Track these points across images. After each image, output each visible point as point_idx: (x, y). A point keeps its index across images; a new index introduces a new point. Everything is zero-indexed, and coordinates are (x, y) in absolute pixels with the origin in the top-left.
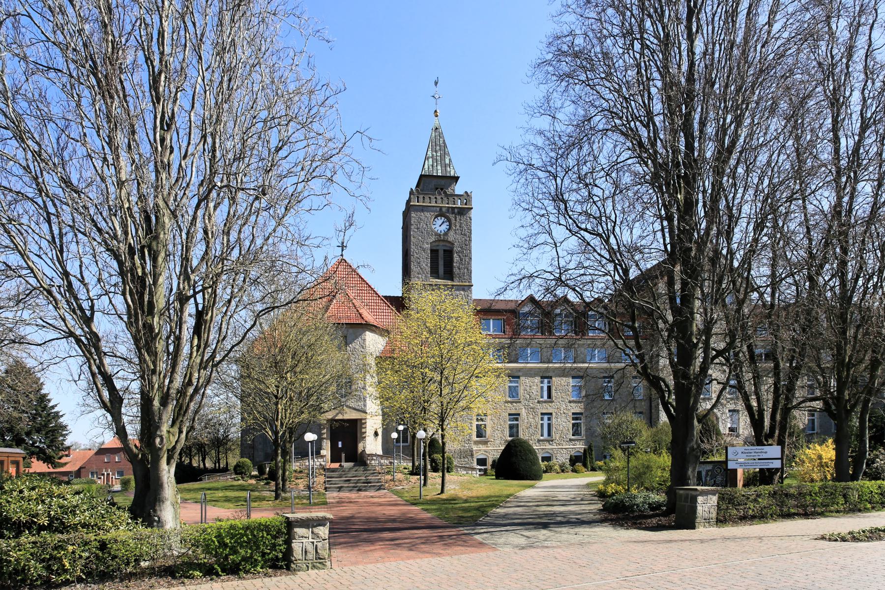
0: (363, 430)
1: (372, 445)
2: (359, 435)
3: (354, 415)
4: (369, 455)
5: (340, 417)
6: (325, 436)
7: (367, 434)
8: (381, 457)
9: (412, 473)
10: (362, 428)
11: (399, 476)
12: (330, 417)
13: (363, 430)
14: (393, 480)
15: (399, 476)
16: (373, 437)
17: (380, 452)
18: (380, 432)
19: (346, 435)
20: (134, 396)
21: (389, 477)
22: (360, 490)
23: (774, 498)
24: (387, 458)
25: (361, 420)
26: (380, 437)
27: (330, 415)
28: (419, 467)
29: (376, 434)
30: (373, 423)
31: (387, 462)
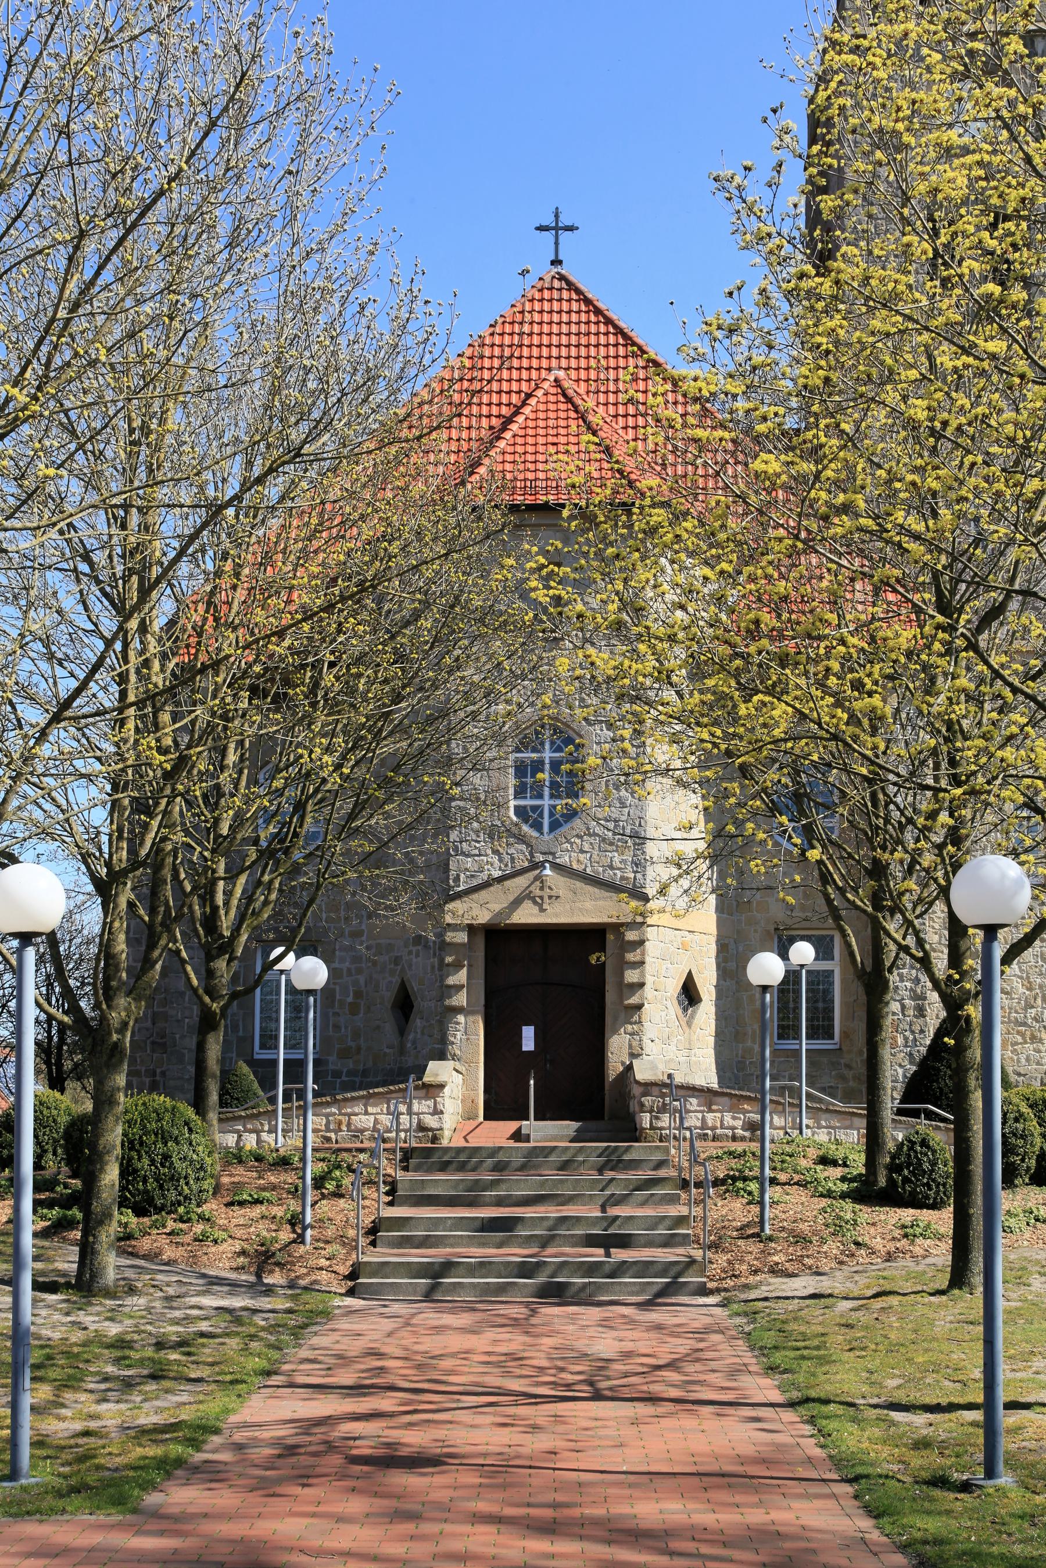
0: (631, 976)
1: (668, 1042)
2: (610, 997)
3: (575, 907)
4: (648, 1086)
5: (526, 915)
6: (461, 999)
7: (648, 991)
8: (706, 1095)
9: (866, 1192)
10: (623, 965)
11: (791, 1206)
12: (483, 917)
13: (631, 976)
14: (754, 1232)
15: (791, 1206)
16: (674, 1009)
17: (707, 1075)
18: (707, 985)
19: (556, 994)
20: (304, 427)
21: (734, 1210)
22: (555, 1293)
23: (643, 954)
24: (735, 1103)
25: (617, 928)
26: (707, 1011)
27: (479, 910)
28: (911, 1158)
29: (689, 994)
30: (678, 942)
31: (734, 1122)
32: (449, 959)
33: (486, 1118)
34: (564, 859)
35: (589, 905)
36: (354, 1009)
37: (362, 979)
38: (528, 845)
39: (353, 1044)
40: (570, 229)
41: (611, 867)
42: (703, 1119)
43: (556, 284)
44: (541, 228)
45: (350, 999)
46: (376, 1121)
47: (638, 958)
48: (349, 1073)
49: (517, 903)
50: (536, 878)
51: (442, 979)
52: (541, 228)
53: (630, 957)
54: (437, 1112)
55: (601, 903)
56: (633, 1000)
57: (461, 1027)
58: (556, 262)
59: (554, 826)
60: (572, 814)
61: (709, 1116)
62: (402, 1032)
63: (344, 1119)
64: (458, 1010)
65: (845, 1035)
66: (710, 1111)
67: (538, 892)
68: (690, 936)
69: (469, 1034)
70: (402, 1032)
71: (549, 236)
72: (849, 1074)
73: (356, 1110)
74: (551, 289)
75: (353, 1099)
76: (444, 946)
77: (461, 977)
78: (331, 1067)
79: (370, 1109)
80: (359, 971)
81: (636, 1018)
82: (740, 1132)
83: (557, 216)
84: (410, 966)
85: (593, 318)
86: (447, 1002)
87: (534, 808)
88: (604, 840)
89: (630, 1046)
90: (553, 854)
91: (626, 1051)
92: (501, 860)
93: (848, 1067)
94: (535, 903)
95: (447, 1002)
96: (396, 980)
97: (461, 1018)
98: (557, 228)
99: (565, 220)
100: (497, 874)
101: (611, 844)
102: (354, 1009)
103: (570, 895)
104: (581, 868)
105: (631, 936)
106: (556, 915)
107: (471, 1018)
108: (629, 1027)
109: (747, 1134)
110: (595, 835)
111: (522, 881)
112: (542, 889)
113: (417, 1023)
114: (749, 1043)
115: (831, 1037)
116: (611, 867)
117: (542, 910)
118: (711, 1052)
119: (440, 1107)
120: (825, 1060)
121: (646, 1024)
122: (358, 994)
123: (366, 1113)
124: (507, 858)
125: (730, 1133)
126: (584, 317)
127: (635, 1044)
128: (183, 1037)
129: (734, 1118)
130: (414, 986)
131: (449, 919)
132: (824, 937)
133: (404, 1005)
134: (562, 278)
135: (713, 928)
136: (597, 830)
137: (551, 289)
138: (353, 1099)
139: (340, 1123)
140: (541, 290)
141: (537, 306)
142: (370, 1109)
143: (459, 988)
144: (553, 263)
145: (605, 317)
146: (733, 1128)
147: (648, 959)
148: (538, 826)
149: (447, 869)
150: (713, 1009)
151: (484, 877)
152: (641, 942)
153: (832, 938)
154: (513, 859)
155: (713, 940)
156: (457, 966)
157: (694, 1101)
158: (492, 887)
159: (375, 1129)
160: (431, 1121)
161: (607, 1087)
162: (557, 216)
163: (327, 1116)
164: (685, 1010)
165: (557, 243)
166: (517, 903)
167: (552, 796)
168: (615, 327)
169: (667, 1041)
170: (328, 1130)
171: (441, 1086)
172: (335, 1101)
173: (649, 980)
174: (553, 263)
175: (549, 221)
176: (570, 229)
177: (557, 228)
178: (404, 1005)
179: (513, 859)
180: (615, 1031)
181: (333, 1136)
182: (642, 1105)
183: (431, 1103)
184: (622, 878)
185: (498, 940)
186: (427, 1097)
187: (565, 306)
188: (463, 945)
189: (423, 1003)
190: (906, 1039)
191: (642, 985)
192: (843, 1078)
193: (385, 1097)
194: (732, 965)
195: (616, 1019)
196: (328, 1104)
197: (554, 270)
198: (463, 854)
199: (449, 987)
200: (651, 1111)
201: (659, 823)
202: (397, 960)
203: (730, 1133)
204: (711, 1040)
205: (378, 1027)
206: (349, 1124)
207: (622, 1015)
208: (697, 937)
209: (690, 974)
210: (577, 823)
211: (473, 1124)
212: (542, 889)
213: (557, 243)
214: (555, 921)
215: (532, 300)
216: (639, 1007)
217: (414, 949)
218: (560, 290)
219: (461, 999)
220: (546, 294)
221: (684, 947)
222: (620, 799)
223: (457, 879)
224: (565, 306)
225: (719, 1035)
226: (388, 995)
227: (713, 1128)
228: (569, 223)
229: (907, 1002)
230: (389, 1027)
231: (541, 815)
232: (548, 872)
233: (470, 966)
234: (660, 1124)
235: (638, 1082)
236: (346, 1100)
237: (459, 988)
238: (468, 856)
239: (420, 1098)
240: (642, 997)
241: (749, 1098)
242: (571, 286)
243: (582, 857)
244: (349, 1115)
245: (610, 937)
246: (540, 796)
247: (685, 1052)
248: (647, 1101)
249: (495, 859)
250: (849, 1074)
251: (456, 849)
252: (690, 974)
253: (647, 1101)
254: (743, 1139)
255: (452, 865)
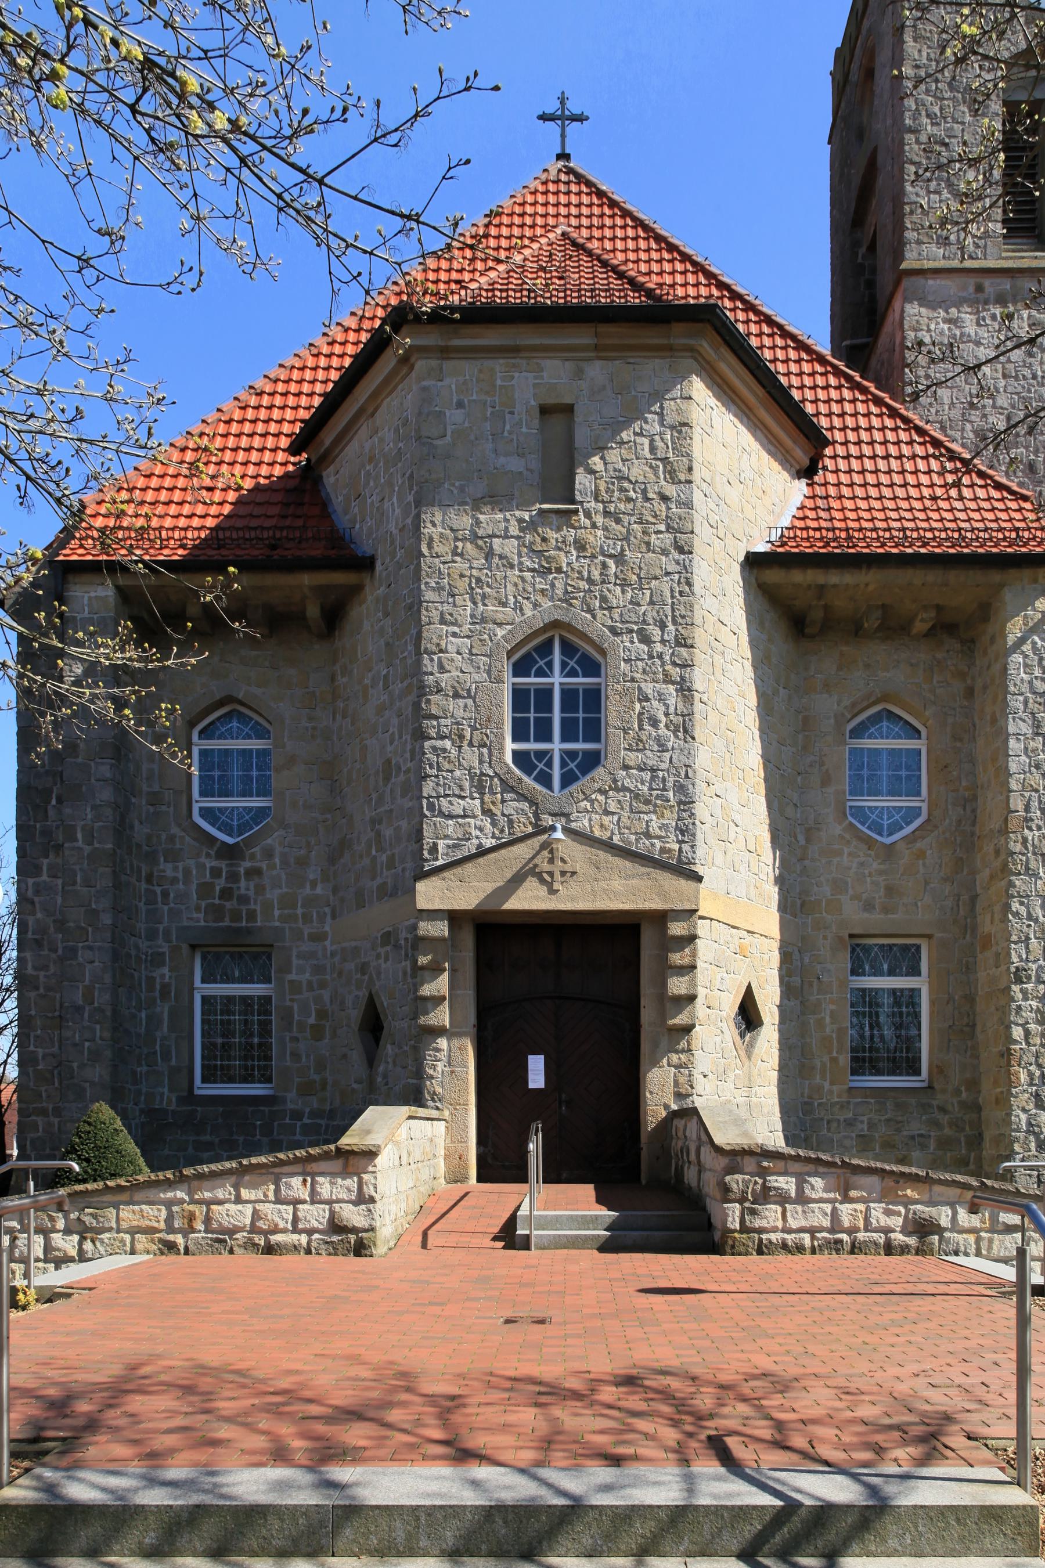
0: (677, 986)
1: (727, 1081)
2: (647, 1015)
5: (530, 899)
6: (442, 1016)
10: (666, 970)
13: (677, 986)
16: (730, 1031)
23: (694, 955)
25: (661, 918)
29: (748, 1016)
32: (423, 960)
33: (480, 1179)
34: (582, 823)
35: (617, 884)
36: (317, 1032)
37: (326, 995)
38: (532, 803)
39: (317, 1077)
40: (580, 118)
41: (648, 835)
42: (835, 1214)
43: (563, 177)
44: (544, 117)
45: (312, 1020)
46: (256, 1214)
47: (686, 961)
48: (313, 1114)
49: (517, 881)
50: (544, 846)
51: (416, 987)
52: (544, 117)
53: (677, 958)
54: (363, 1199)
55: (635, 882)
56: (680, 1020)
57: (443, 1055)
58: (563, 156)
59: (568, 780)
60: (592, 761)
61: (846, 1210)
62: (371, 1060)
63: (199, 1211)
64: (439, 1031)
65: (938, 1069)
66: (847, 1199)
67: (546, 866)
68: (749, 938)
69: (454, 1065)
70: (371, 1060)
71: (553, 127)
72: (944, 1119)
73: (220, 1194)
74: (557, 182)
75: (213, 1175)
76: (419, 943)
77: (441, 985)
78: (290, 1106)
79: (245, 1194)
80: (323, 985)
81: (683, 1044)
82: (898, 1237)
83: (563, 103)
84: (379, 973)
85: (607, 211)
86: (422, 1020)
87: (541, 755)
88: (637, 796)
89: (676, 1083)
90: (567, 816)
91: (670, 1089)
92: (494, 824)
93: (942, 1109)
94: (542, 881)
95: (422, 1020)
96: (363, 994)
97: (443, 1043)
98: (562, 117)
99: (574, 107)
100: (489, 842)
101: (647, 802)
102: (317, 1032)
103: (592, 871)
104: (605, 835)
105: (676, 929)
106: (573, 900)
107: (456, 1042)
108: (675, 1058)
109: (912, 1241)
110: (625, 789)
111: (523, 851)
112: (551, 861)
113: (389, 1049)
114: (818, 1080)
115: (918, 1073)
116: (648, 835)
117: (552, 892)
118: (774, 1090)
119: (369, 1190)
120: (913, 1101)
121: (698, 1053)
122: (322, 1014)
123: (238, 1200)
124: (503, 821)
125: (881, 1238)
126: (596, 211)
127: (682, 1080)
128: (82, 1066)
129: (888, 1213)
130: (384, 1001)
131: (422, 903)
132: (905, 948)
133: (373, 1025)
134: (570, 171)
135: (776, 932)
136: (627, 783)
137: (557, 182)
138: (213, 1175)
139: (191, 1217)
140: (545, 183)
141: (541, 199)
142: (245, 1194)
143: (439, 1000)
144: (559, 157)
145: (621, 209)
146: (887, 1231)
147: (700, 964)
148: (545, 779)
149: (418, 836)
150: (776, 1036)
151: (471, 847)
152: (692, 938)
153: (918, 948)
154: (511, 823)
155: (775, 945)
156: (436, 970)
157: (818, 1182)
158: (480, 852)
159: (254, 1229)
160: (353, 1215)
161: (644, 1139)
162: (563, 103)
163: (169, 1204)
164: (742, 1035)
165: (563, 136)
166: (517, 881)
167: (564, 739)
168: (634, 219)
169: (722, 1076)
170: (170, 1229)
171: (371, 1154)
172: (182, 1179)
173: (701, 992)
174: (559, 157)
175: (552, 107)
176: (580, 118)
177: (562, 117)
178: (373, 1025)
179: (511, 823)
180: (655, 1063)
181: (179, 1239)
182: (726, 1189)
183: (352, 1183)
184: (663, 850)
185: (496, 938)
186: (345, 1174)
187: (574, 199)
188: (442, 939)
189: (395, 1024)
190: (1031, 1075)
191: (692, 998)
192: (936, 1124)
193: (274, 1173)
194: (796, 980)
195: (656, 1045)
196: (169, 1184)
197: (560, 164)
198: (441, 814)
199: (425, 999)
200: (741, 1201)
201: (711, 777)
202: (363, 968)
203: (881, 1238)
204: (775, 1075)
205: (345, 1056)
206: (208, 1220)
207: (664, 1042)
208: (757, 940)
209: (749, 988)
210: (599, 772)
211: (459, 1189)
212: (551, 861)
213: (563, 136)
214: (570, 906)
215: (534, 193)
216: (688, 1029)
217: (382, 951)
218: (568, 183)
219: (442, 1016)
220: (552, 187)
221: (742, 952)
222: (658, 740)
223: (434, 849)
224: (574, 199)
225: (783, 1069)
226: (355, 1014)
227: (852, 1231)
228: (576, 111)
229: (1032, 1026)
230: (357, 1056)
231: (549, 764)
232: (559, 835)
233: (453, 971)
234: (758, 1223)
235: (718, 1150)
236: (200, 1177)
237: (439, 1000)
238: (450, 817)
239: (333, 1175)
240: (692, 1015)
241: (914, 1179)
242: (580, 179)
243: (606, 820)
244: (208, 1203)
245: (647, 938)
246: (549, 739)
247: (744, 1091)
248: (736, 1181)
249: (487, 823)
250: (944, 1119)
251: (431, 807)
252: (749, 988)
253: (736, 1181)
254: (904, 1250)
255: (427, 832)
